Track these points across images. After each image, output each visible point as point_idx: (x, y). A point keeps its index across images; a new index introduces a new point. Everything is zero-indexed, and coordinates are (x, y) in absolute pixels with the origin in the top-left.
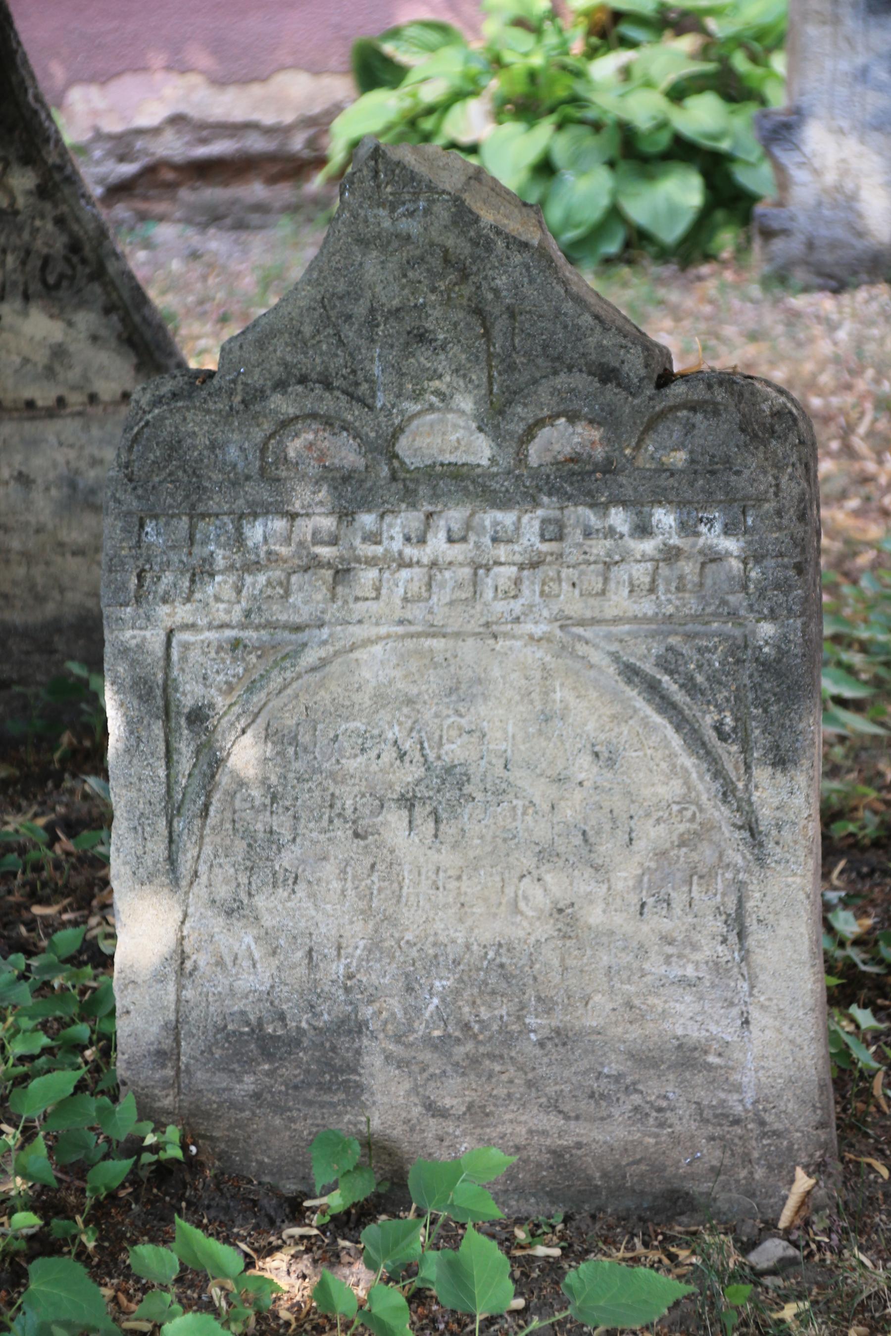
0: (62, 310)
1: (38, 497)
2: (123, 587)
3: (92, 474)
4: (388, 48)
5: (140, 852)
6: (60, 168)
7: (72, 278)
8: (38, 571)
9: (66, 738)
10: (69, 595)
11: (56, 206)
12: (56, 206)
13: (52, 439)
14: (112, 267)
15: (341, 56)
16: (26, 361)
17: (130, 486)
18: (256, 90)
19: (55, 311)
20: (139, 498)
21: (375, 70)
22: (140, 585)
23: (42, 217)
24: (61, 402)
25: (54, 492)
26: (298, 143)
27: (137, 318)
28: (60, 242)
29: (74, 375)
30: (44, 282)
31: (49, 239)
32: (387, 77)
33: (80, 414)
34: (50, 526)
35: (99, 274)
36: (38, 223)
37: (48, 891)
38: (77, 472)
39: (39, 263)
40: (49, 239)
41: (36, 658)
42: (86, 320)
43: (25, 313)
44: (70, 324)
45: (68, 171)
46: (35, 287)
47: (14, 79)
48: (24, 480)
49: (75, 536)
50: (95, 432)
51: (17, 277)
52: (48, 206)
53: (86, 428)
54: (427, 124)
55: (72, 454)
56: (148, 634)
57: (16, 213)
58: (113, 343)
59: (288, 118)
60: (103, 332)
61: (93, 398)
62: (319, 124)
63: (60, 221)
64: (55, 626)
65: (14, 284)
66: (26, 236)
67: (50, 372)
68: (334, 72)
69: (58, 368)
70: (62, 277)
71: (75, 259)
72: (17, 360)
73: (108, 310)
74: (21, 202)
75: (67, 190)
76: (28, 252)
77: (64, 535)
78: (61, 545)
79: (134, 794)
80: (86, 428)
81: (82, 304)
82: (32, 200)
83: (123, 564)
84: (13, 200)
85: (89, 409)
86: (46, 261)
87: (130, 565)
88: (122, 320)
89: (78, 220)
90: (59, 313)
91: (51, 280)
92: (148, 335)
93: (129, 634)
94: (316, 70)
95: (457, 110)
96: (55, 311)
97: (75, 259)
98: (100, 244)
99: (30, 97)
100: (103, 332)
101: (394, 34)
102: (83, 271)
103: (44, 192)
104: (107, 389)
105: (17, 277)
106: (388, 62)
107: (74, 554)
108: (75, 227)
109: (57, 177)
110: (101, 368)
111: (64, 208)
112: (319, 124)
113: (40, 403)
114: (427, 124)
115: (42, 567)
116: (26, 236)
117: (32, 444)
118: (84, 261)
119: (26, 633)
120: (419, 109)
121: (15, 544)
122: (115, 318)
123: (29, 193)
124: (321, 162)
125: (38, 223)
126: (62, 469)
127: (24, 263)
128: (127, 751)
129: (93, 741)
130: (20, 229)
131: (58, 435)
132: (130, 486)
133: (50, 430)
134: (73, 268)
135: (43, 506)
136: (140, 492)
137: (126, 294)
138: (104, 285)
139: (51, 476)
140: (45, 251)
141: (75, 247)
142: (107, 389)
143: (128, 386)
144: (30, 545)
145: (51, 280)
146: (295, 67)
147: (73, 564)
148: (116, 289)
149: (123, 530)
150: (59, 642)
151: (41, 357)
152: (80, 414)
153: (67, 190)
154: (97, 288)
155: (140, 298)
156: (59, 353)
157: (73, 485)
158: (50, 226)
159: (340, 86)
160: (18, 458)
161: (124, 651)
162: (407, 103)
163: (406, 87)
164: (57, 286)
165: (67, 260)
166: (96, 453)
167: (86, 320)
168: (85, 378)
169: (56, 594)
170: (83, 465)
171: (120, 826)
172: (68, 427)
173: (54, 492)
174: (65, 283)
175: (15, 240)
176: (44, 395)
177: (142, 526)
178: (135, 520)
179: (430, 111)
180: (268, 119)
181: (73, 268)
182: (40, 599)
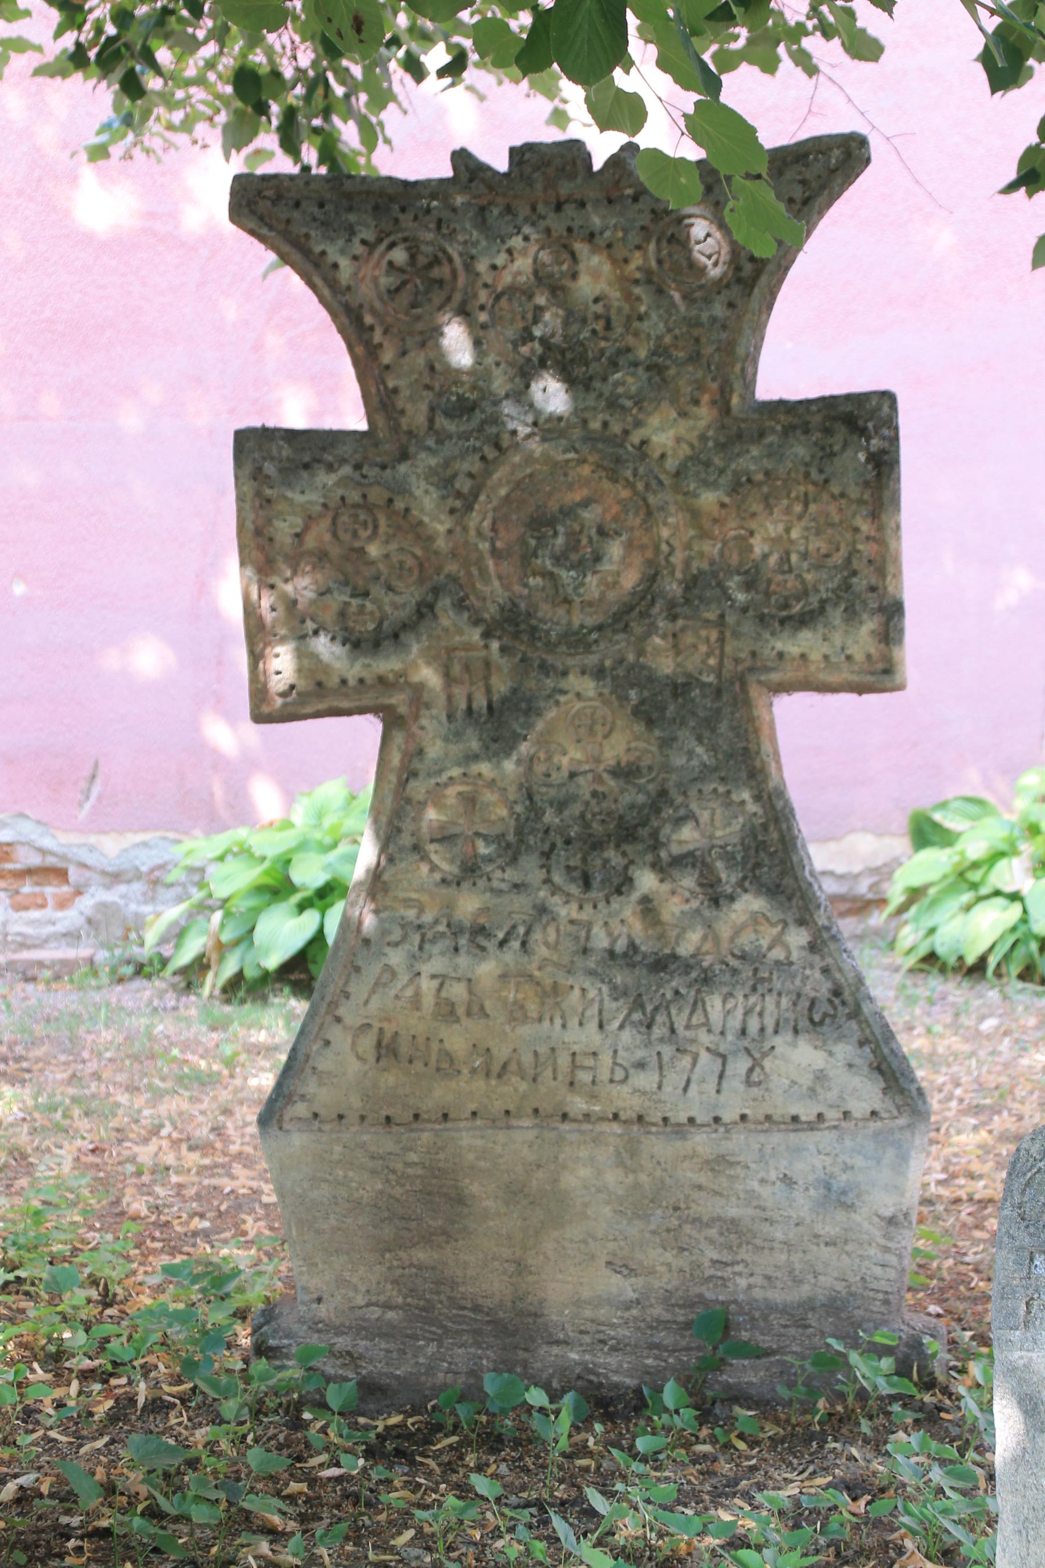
0: (824, 1042)
1: (798, 1195)
2: (1013, 1313)
3: (844, 1177)
4: (937, 817)
5: (1024, 1554)
6: (828, 929)
7: (834, 1016)
8: (796, 1257)
9: (821, 1404)
10: (821, 1278)
11: (823, 958)
12: (823, 958)
13: (812, 1147)
14: (866, 1008)
15: (901, 822)
16: (794, 1082)
17: (1023, 1224)
18: (832, 846)
19: (819, 1043)
20: (1031, 1235)
21: (925, 833)
22: (1029, 1312)
23: (812, 967)
24: (820, 1116)
25: (812, 1192)
26: (863, 888)
27: (886, 1051)
28: (825, 988)
29: (832, 1096)
30: (811, 1020)
31: (818, 986)
32: (936, 839)
33: (835, 1127)
34: (808, 1220)
35: (856, 1013)
36: (808, 972)
37: (850, 1552)
38: (832, 1176)
39: (807, 1004)
40: (818, 986)
41: (792, 1331)
42: (845, 1050)
43: (794, 1045)
44: (831, 1054)
45: (834, 930)
46: (803, 1023)
47: (795, 859)
48: (787, 1180)
49: (829, 1229)
50: (848, 1143)
51: (790, 1015)
52: (817, 958)
53: (840, 1139)
54: (975, 876)
55: (828, 1161)
56: (1034, 1355)
57: (791, 964)
58: (866, 1070)
59: (857, 868)
60: (858, 1061)
61: (846, 1114)
62: (884, 872)
63: (825, 971)
64: (809, 1305)
65: (787, 1020)
66: (798, 982)
67: (812, 1091)
68: (892, 834)
69: (819, 1090)
70: (825, 1015)
71: (837, 1001)
72: (787, 1082)
73: (861, 1044)
74: (795, 956)
75: (832, 946)
76: (799, 995)
77: (819, 1228)
78: (817, 1236)
79: (1020, 1500)
80: (840, 1139)
81: (841, 1038)
82: (804, 953)
83: (1014, 1292)
84: (789, 953)
85: (843, 1124)
86: (813, 1003)
87: (1021, 1294)
88: (873, 1052)
89: (840, 970)
90: (821, 1046)
91: (817, 1018)
92: (895, 1065)
93: (1017, 1354)
94: (879, 834)
95: (1002, 864)
96: (819, 1043)
97: (837, 1001)
98: (858, 989)
99: (807, 873)
100: (858, 1061)
101: (943, 805)
102: (843, 1011)
103: (813, 947)
104: (859, 1108)
105: (790, 1015)
106: (936, 826)
107: (827, 1244)
108: (838, 976)
109: (825, 935)
110: (855, 1090)
111: (829, 960)
112: (884, 872)
113: (803, 1118)
114: (975, 876)
115: (800, 1255)
116: (798, 982)
117: (797, 1151)
118: (843, 1003)
119: (784, 1310)
120: (967, 864)
121: (779, 1235)
122: (867, 1049)
123: (803, 948)
124: (883, 902)
125: (808, 972)
126: (820, 1174)
127: (795, 1004)
128: (1014, 1460)
129: (846, 1408)
130: (793, 977)
131: (817, 1144)
132: (1023, 1224)
133: (809, 1140)
134: (835, 1008)
135: (802, 1204)
136: (1032, 1229)
137: (878, 1031)
138: (859, 1023)
139: (811, 1178)
140: (813, 994)
141: (837, 992)
142: (859, 1108)
143: (877, 1107)
144: (791, 1235)
145: (817, 1018)
146: (864, 829)
147: (825, 1252)
148: (869, 1026)
149: (1015, 1262)
150: (812, 1319)
151: (806, 1080)
152: (835, 1127)
153: (832, 946)
154: (853, 1025)
155: (889, 1036)
156: (820, 1077)
157: (828, 1187)
158: (818, 975)
159: (901, 845)
160: (784, 1163)
161: (1012, 1370)
162: (956, 858)
163: (958, 847)
164: (821, 1023)
165: (830, 1001)
166: (848, 1161)
167: (845, 1050)
168: (841, 1098)
169: (810, 1277)
170: (837, 1170)
171: (1006, 1527)
172: (824, 1138)
173: (812, 1192)
174: (828, 1021)
175: (789, 985)
176: (807, 1112)
177: (1032, 1260)
178: (1027, 1254)
179: (975, 865)
180: (840, 869)
181: (835, 1008)
182: (798, 1282)
